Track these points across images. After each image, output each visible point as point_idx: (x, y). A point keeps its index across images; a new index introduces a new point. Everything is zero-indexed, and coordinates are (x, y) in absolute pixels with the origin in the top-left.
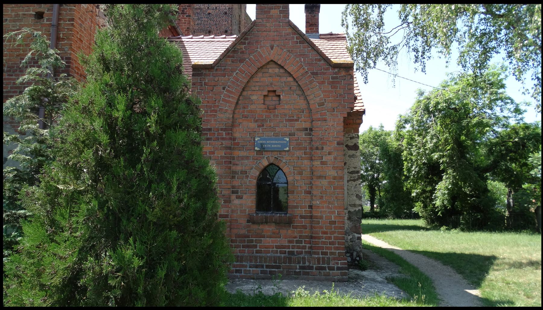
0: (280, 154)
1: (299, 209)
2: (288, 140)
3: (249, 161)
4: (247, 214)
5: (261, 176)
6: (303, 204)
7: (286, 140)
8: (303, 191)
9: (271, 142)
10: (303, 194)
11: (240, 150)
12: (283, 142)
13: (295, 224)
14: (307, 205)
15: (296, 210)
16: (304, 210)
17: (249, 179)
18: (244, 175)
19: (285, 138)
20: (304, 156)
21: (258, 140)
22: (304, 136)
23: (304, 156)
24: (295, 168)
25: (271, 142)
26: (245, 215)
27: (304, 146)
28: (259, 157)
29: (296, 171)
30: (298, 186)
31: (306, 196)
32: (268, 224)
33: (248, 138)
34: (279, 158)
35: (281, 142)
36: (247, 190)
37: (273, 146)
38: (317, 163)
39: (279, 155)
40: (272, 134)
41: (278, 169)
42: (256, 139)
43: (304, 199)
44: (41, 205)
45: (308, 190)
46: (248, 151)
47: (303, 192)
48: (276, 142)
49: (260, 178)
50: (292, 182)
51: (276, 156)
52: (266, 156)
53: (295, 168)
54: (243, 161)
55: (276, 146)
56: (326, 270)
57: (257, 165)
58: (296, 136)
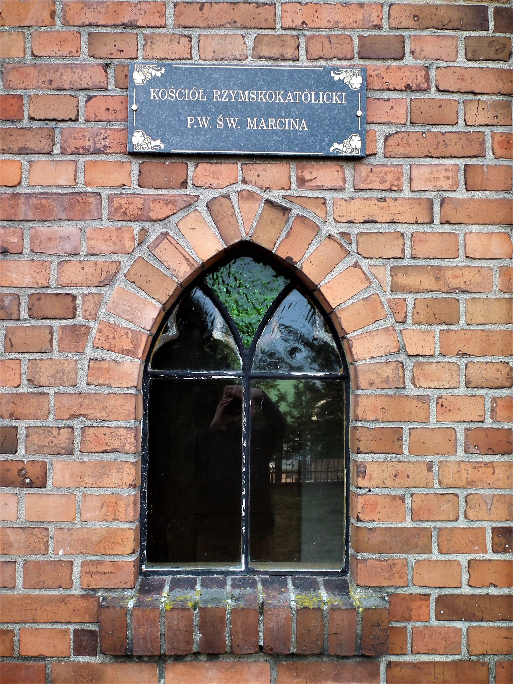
0: (302, 182)
1: (436, 555)
2: (356, 82)
3: (91, 225)
4: (76, 591)
5: (173, 332)
6: (462, 523)
7: (342, 86)
8: (460, 428)
9: (245, 96)
10: (461, 453)
11: (22, 152)
12: (323, 98)
13: (408, 658)
14: (488, 526)
15: (412, 558)
16: (463, 559)
17: (89, 351)
18: (56, 324)
19: (337, 70)
20: (461, 194)
21: (154, 82)
22: (461, 61)
23: (461, 194)
24: (402, 280)
25: (245, 96)
26: (63, 600)
27: (461, 128)
28: (157, 199)
29: (411, 298)
30: (424, 399)
31: (477, 466)
32: (223, 661)
33: (83, 67)
34: (296, 211)
35: (311, 98)
36: (77, 425)
37: (252, 124)
38: (80, 74)
39: (295, 191)
40: (250, 41)
41: (280, 283)
42: (138, 78)
43: (470, 484)
44: (321, 117)
45: (489, 423)
46: (82, 159)
47: (461, 438)
48: (278, 97)
49: (168, 345)
50: (389, 371)
51: (275, 196)
52: (207, 195)
53: (402, 280)
54: (43, 228)
55: (273, 124)
56: (431, 552)
57: (141, 253)
58: (409, 60)
